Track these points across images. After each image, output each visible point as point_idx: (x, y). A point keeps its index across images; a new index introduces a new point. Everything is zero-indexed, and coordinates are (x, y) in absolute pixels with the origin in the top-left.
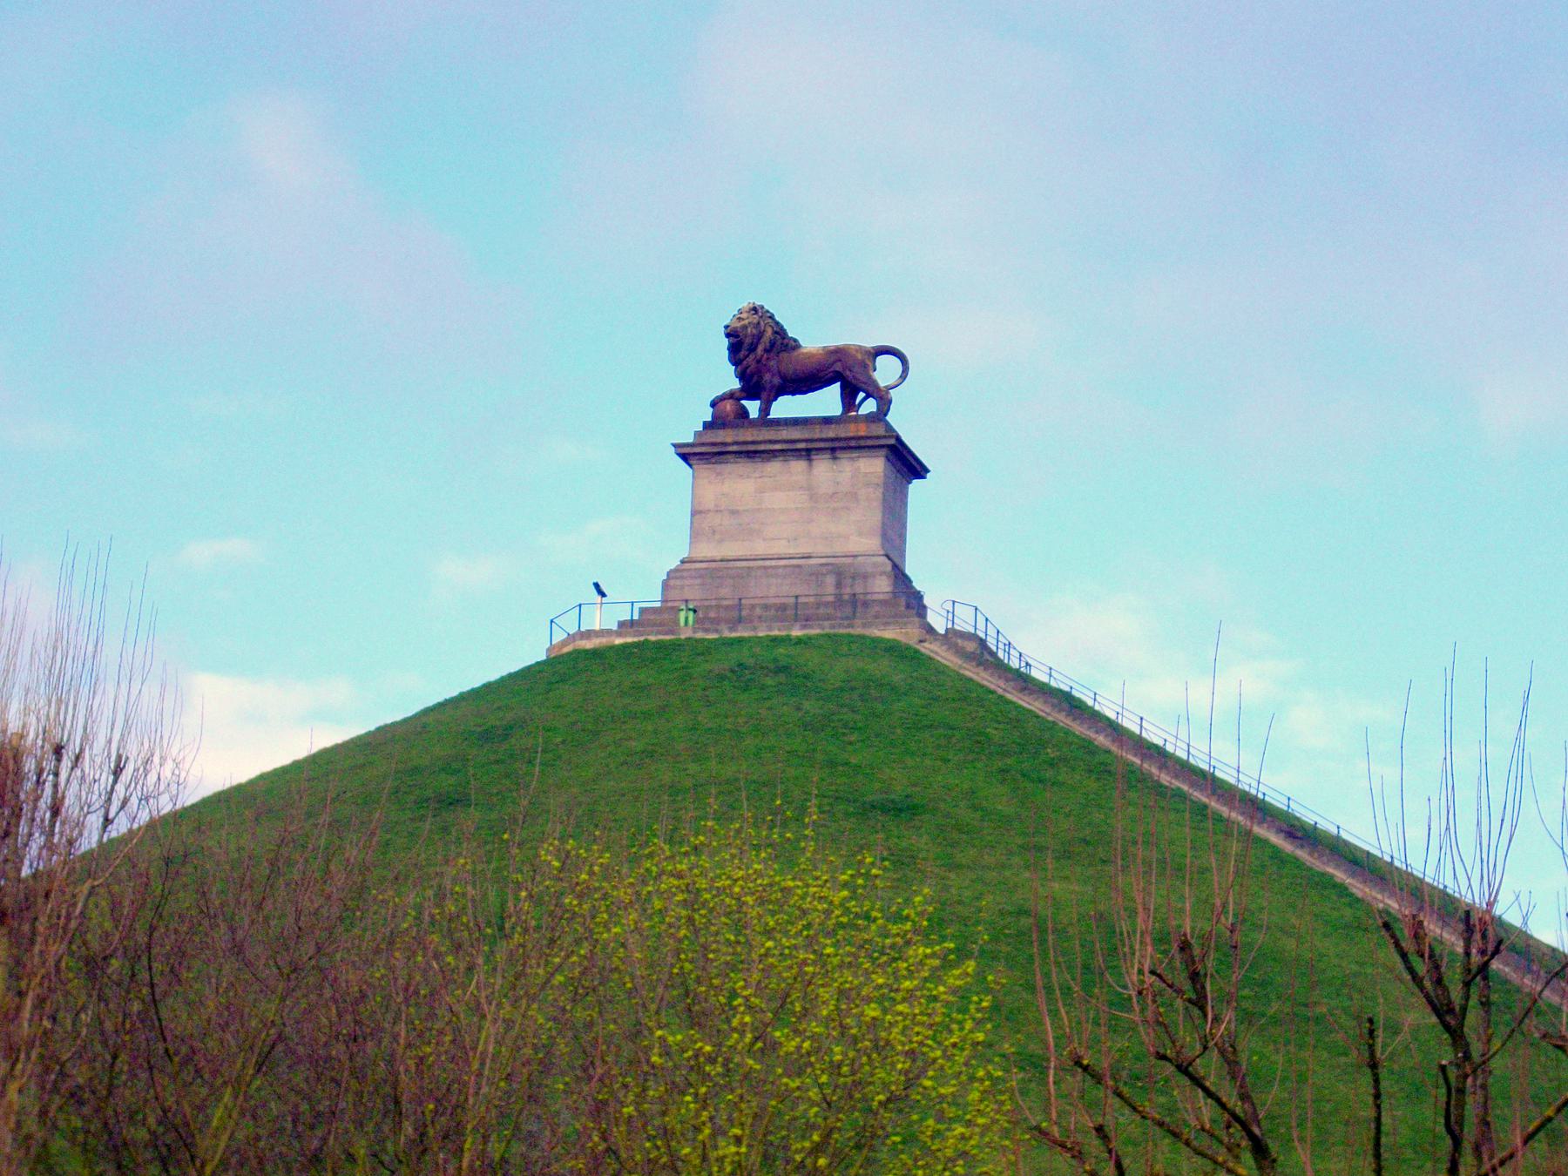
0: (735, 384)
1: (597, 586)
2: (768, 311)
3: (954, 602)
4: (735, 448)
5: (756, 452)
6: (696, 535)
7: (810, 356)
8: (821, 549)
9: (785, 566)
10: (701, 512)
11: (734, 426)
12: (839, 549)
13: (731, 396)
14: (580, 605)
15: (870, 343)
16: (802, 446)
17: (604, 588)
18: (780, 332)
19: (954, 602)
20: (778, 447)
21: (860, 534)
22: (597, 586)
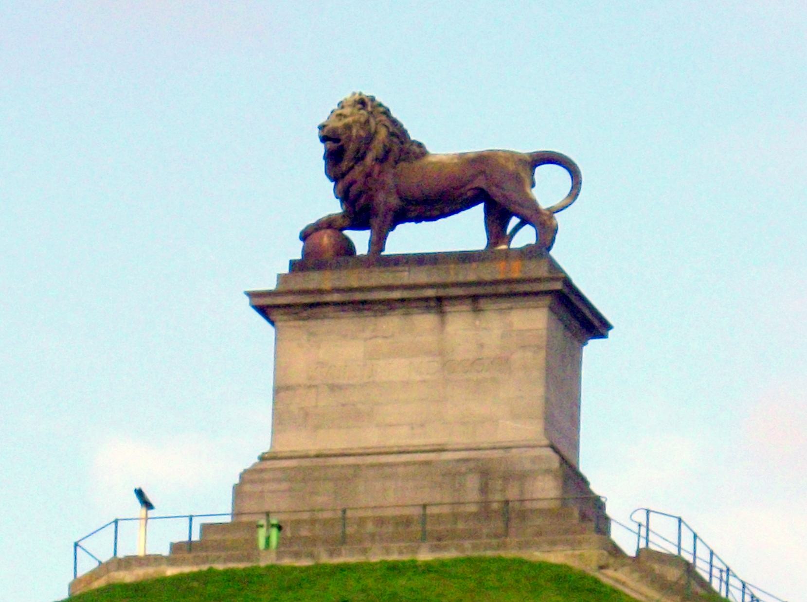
0: (335, 207)
1: (140, 493)
2: (380, 105)
3: (648, 512)
4: (336, 297)
5: (364, 302)
6: (279, 419)
7: (441, 165)
8: (459, 437)
9: (406, 464)
10: (288, 388)
11: (338, 267)
12: (484, 438)
13: (328, 224)
14: (116, 522)
15: (526, 147)
16: (430, 293)
17: (150, 496)
18: (398, 133)
19: (648, 512)
20: (396, 295)
21: (515, 416)
22: (140, 493)
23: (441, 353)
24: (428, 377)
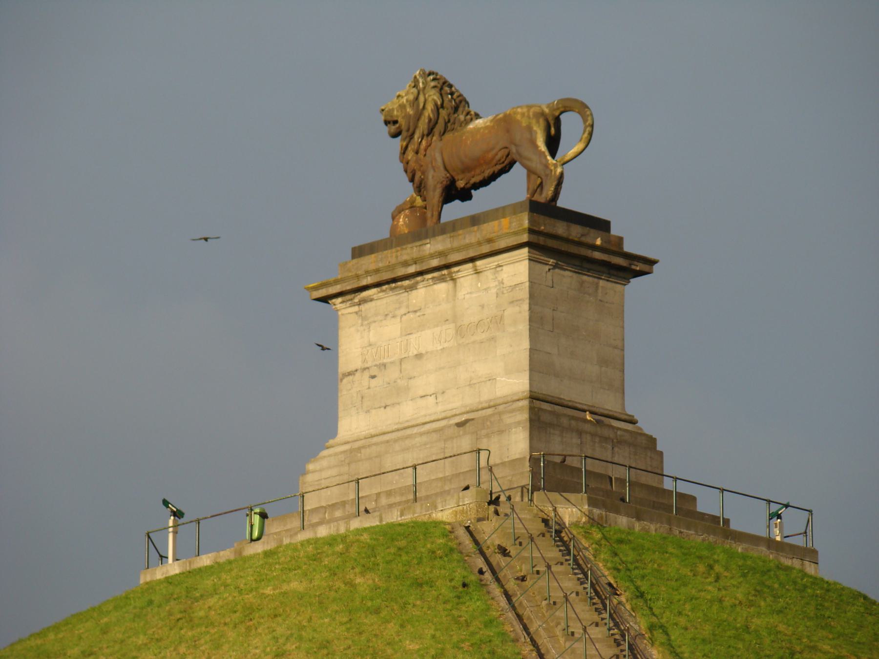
14: (198, 521)
21: (508, 372)
23: (455, 319)
24: (446, 345)
